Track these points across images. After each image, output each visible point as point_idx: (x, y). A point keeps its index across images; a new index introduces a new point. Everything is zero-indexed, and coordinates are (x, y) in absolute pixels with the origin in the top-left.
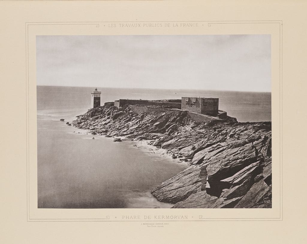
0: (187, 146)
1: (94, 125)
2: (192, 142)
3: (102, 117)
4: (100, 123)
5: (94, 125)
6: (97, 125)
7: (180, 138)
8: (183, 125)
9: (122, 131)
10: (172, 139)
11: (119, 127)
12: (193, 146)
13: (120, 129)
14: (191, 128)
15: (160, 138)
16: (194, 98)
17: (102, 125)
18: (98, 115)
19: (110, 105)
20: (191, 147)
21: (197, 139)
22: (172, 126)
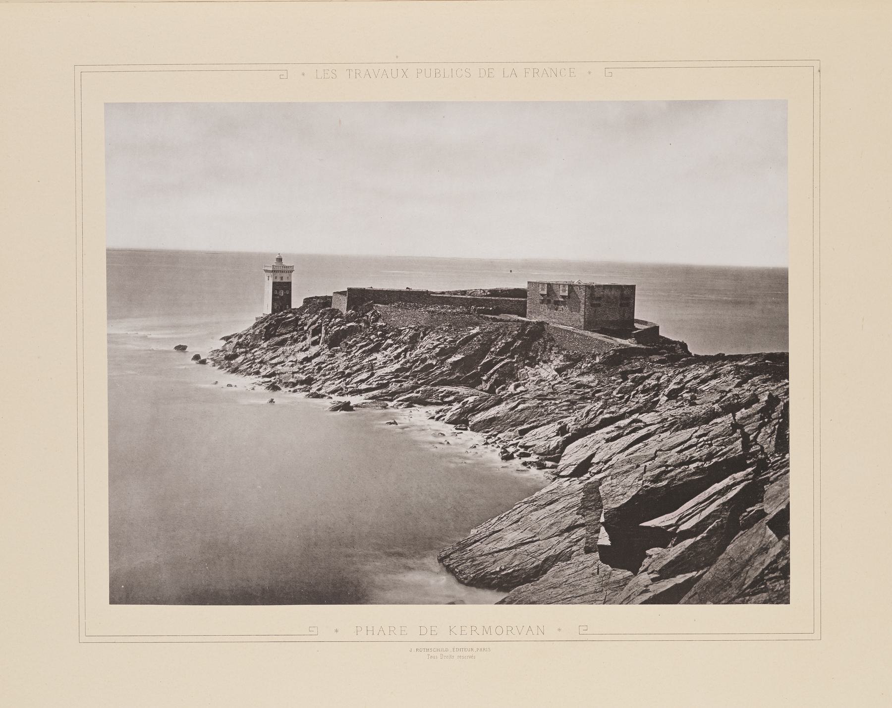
0: (544, 425)
1: (273, 361)
2: (557, 411)
3: (297, 338)
4: (291, 358)
5: (273, 361)
6: (283, 362)
7: (524, 402)
8: (533, 363)
9: (354, 381)
10: (499, 402)
11: (347, 368)
12: (560, 423)
13: (349, 375)
14: (556, 370)
15: (466, 400)
16: (564, 285)
17: (296, 362)
18: (286, 334)
19: (320, 305)
20: (555, 426)
21: (573, 403)
22: (501, 367)
